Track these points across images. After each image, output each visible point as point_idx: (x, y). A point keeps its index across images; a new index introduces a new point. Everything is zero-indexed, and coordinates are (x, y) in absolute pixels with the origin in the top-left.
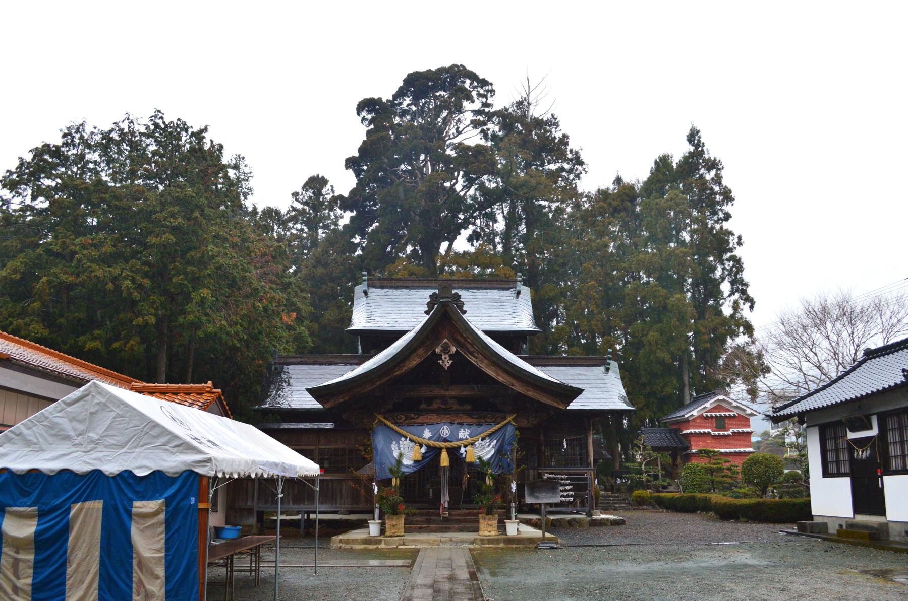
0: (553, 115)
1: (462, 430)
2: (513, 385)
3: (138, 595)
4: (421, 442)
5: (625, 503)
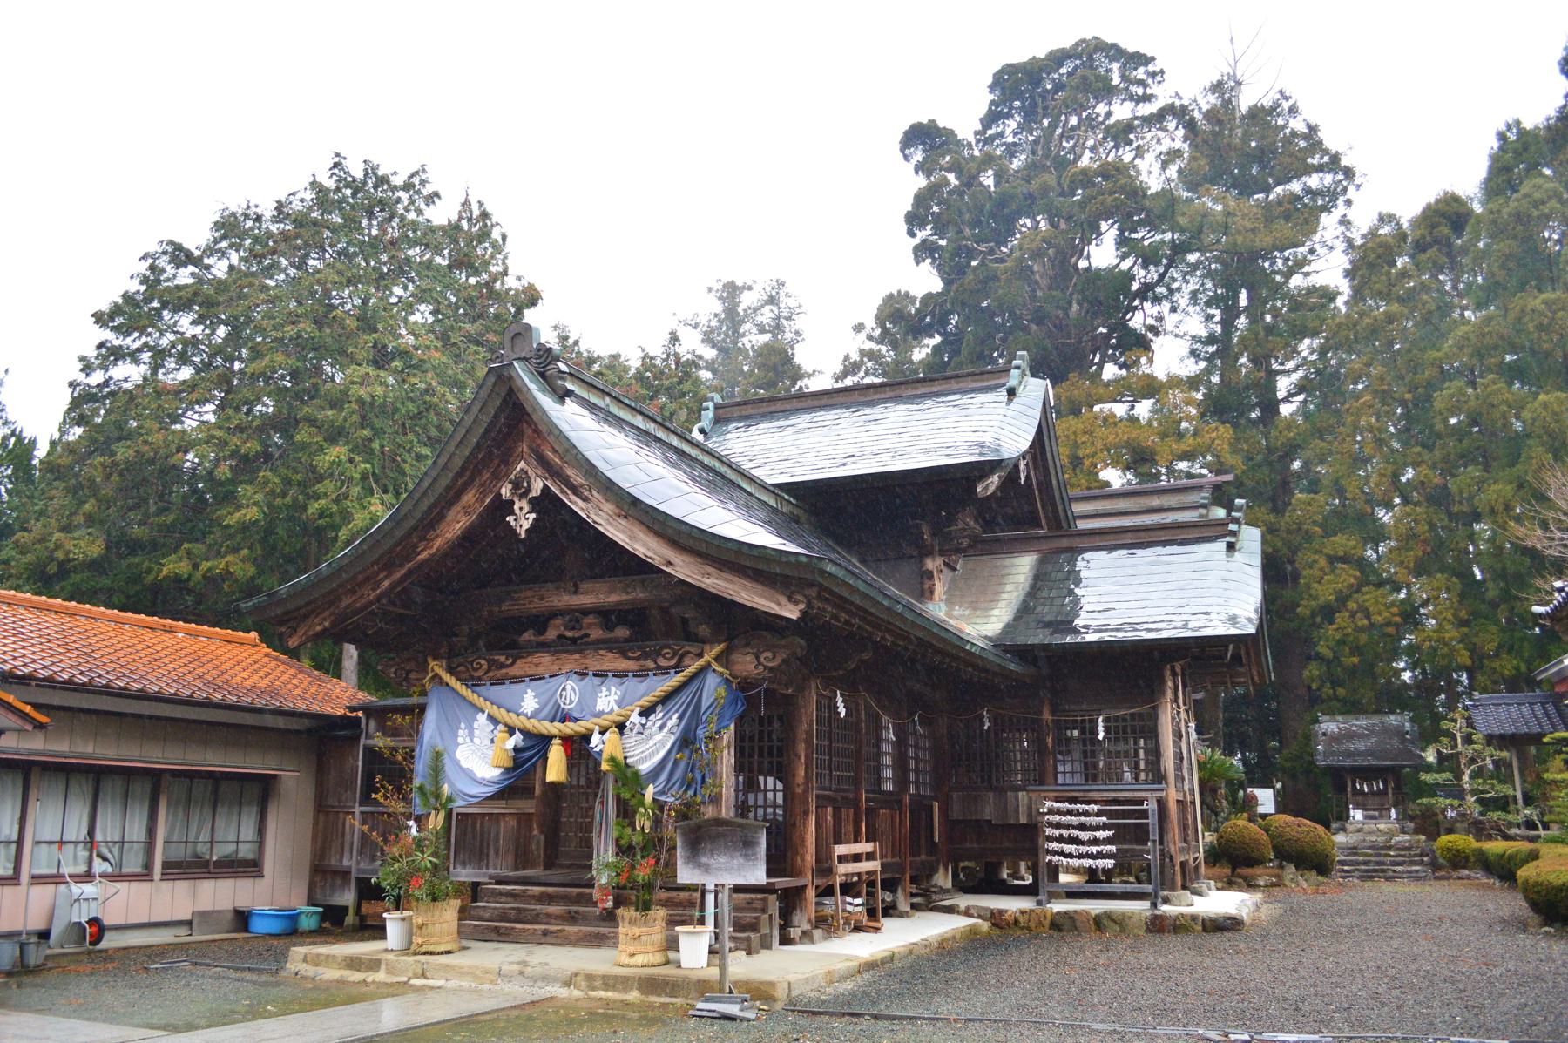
0: (1281, 92)
1: (604, 689)
2: (669, 563)
4: (510, 722)
5: (1421, 863)
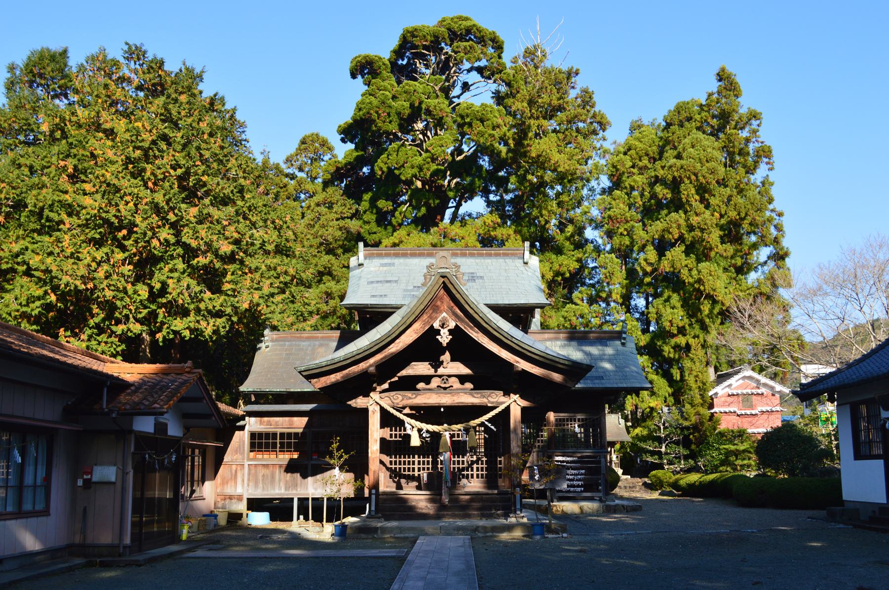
3: (568, 486)
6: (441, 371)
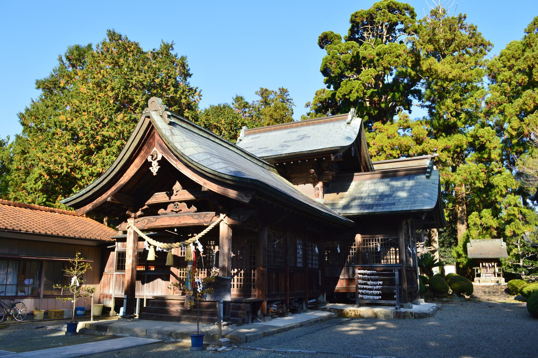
6: (173, 198)
